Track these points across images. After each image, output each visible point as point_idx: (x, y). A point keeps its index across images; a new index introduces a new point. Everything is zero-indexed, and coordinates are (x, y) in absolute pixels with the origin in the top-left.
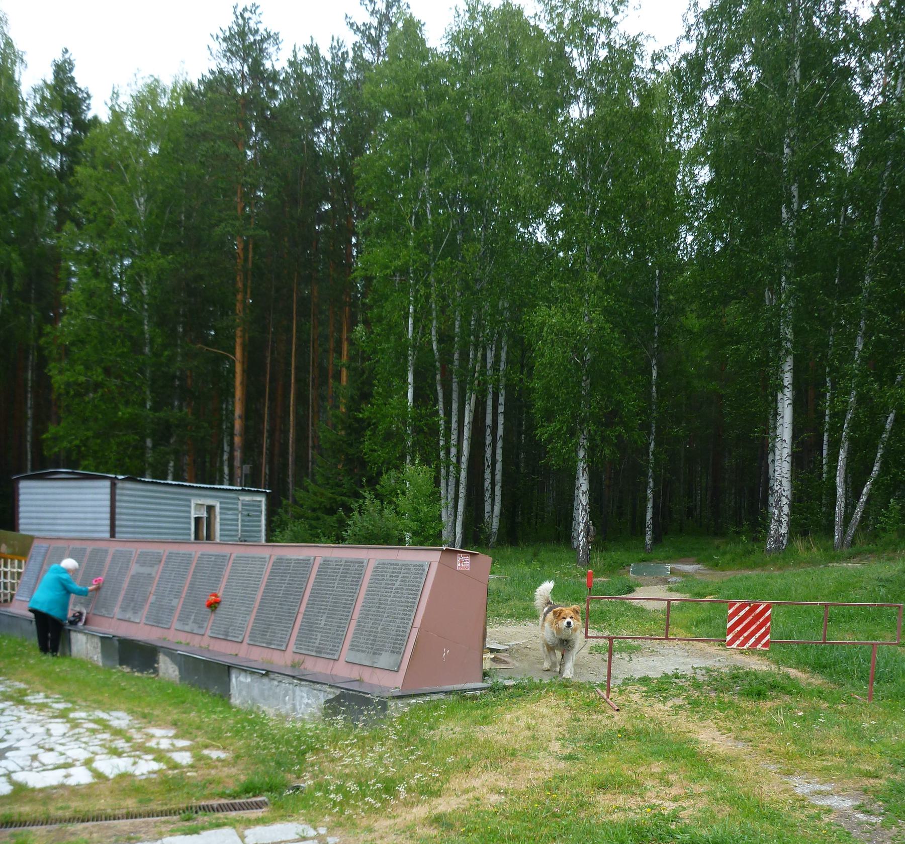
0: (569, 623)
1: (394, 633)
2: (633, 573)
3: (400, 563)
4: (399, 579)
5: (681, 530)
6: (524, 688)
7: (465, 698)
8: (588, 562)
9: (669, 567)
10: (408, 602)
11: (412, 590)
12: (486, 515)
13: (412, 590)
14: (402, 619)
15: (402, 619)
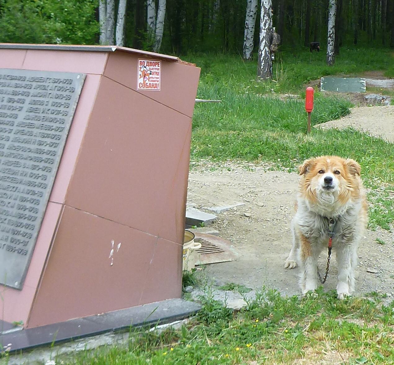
0: (328, 181)
1: (15, 211)
2: (325, 87)
3: (28, 76)
4: (26, 106)
5: (356, 42)
6: (265, 314)
7: (153, 341)
8: (271, 74)
9: (364, 81)
10: (41, 152)
11: (50, 129)
12: (149, 21)
13: (50, 129)
14: (29, 184)
15: (29, 184)
